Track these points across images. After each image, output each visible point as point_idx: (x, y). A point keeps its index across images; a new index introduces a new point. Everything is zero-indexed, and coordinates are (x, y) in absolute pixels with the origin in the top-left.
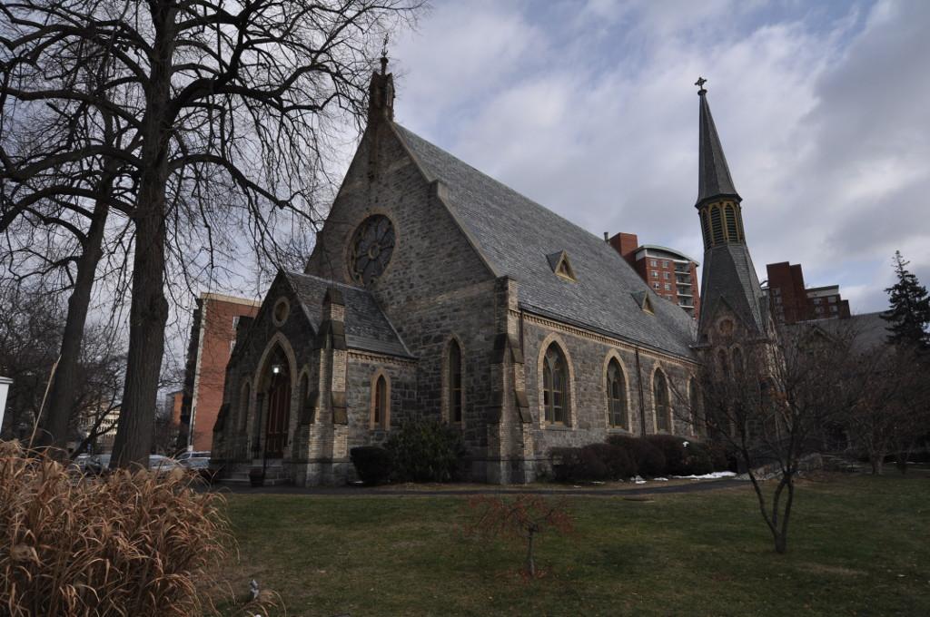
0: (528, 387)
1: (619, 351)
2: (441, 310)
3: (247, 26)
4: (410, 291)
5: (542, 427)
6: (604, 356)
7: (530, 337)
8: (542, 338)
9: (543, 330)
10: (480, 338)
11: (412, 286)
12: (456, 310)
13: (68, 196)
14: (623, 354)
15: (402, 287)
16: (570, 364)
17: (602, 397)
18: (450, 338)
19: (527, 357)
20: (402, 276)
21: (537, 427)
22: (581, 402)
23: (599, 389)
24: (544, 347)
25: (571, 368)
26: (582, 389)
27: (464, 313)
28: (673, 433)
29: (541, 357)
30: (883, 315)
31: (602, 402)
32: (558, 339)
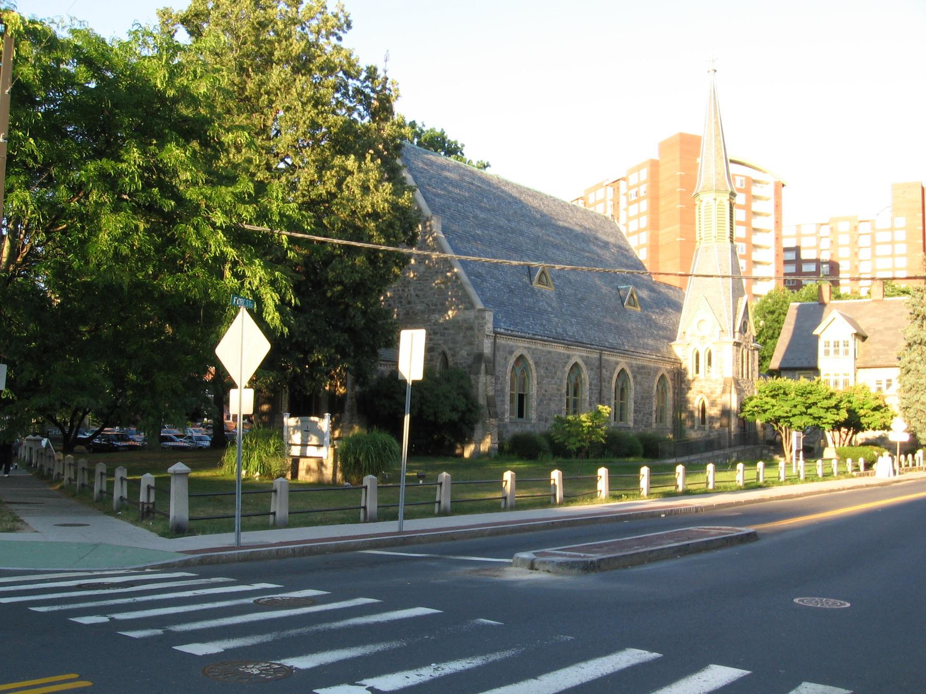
0: (496, 391)
1: (581, 357)
2: (435, 327)
3: (462, 455)
4: (408, 306)
5: (507, 420)
6: (566, 363)
7: (501, 352)
8: (511, 352)
9: (512, 347)
10: (464, 353)
11: (409, 303)
12: (446, 329)
13: (46, 197)
14: (587, 361)
15: (401, 302)
16: (534, 371)
17: (561, 395)
18: (440, 351)
19: (498, 369)
20: (401, 292)
21: (502, 420)
22: (541, 401)
23: (558, 390)
24: (512, 361)
25: (535, 375)
26: (543, 391)
27: (452, 331)
28: (631, 424)
29: (510, 368)
30: (23, 526)
31: (561, 401)
32: (525, 353)
